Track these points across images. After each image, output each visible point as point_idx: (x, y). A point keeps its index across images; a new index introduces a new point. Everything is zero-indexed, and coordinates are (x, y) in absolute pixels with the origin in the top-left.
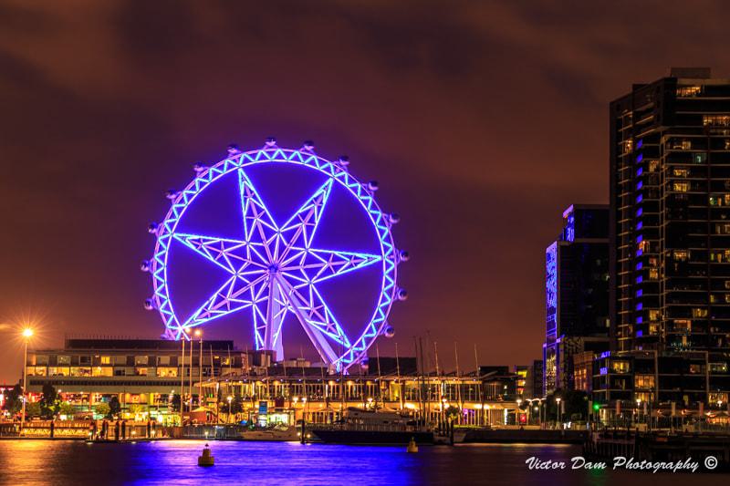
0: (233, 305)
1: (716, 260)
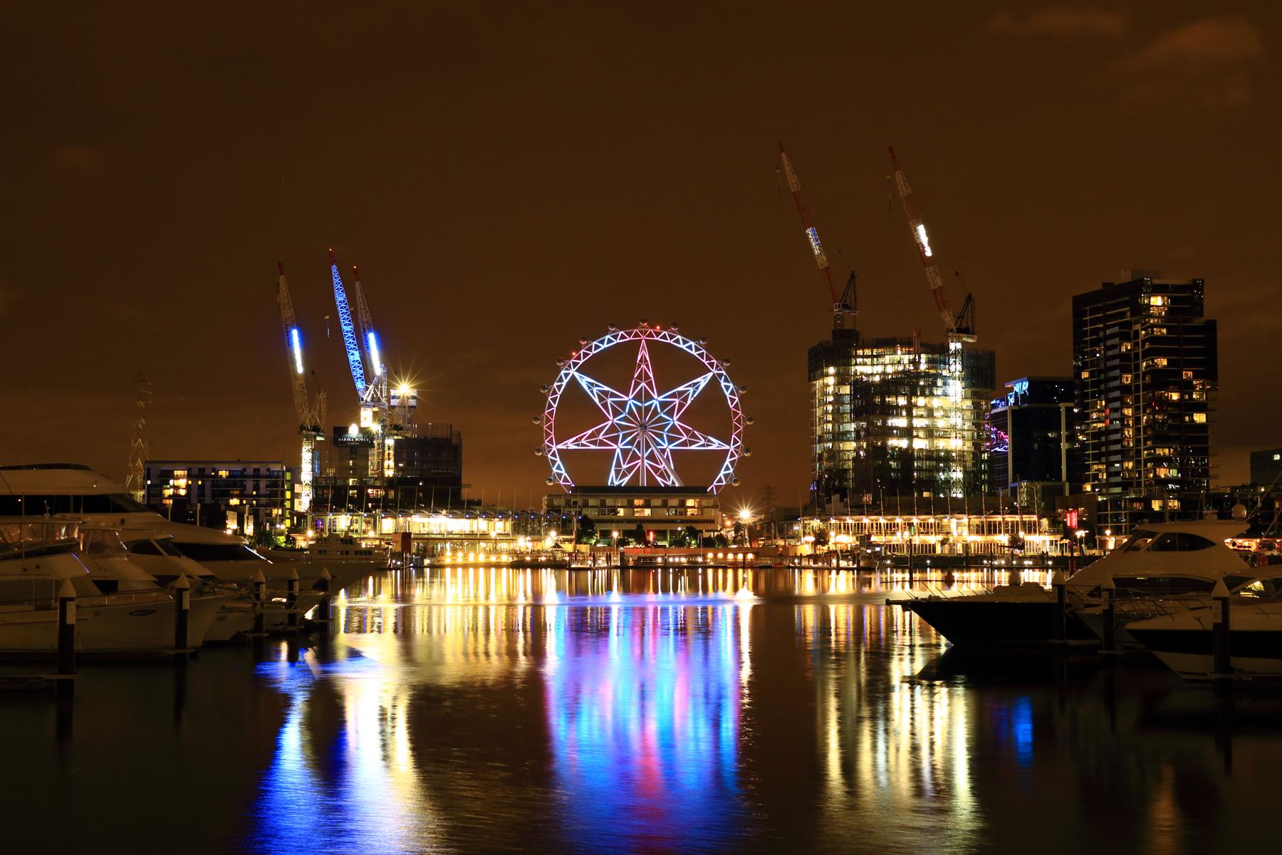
0: (602, 443)
1: (240, 532)
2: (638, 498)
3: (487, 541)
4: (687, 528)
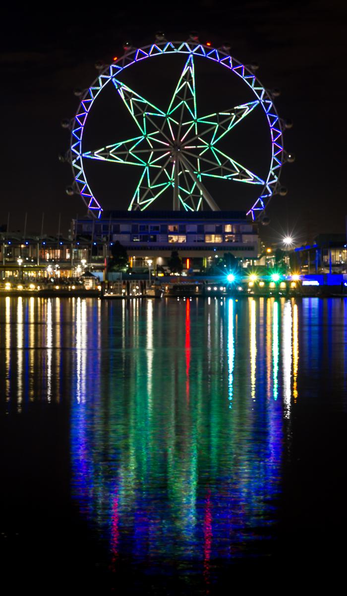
2: (172, 223)
3: (12, 269)
4: (225, 255)
